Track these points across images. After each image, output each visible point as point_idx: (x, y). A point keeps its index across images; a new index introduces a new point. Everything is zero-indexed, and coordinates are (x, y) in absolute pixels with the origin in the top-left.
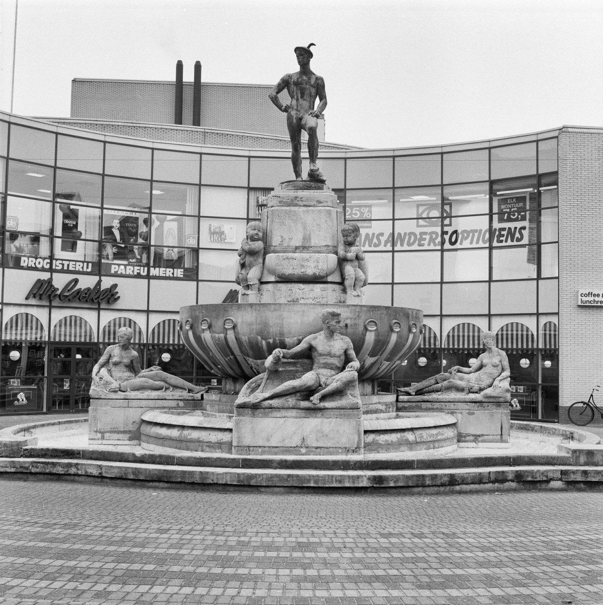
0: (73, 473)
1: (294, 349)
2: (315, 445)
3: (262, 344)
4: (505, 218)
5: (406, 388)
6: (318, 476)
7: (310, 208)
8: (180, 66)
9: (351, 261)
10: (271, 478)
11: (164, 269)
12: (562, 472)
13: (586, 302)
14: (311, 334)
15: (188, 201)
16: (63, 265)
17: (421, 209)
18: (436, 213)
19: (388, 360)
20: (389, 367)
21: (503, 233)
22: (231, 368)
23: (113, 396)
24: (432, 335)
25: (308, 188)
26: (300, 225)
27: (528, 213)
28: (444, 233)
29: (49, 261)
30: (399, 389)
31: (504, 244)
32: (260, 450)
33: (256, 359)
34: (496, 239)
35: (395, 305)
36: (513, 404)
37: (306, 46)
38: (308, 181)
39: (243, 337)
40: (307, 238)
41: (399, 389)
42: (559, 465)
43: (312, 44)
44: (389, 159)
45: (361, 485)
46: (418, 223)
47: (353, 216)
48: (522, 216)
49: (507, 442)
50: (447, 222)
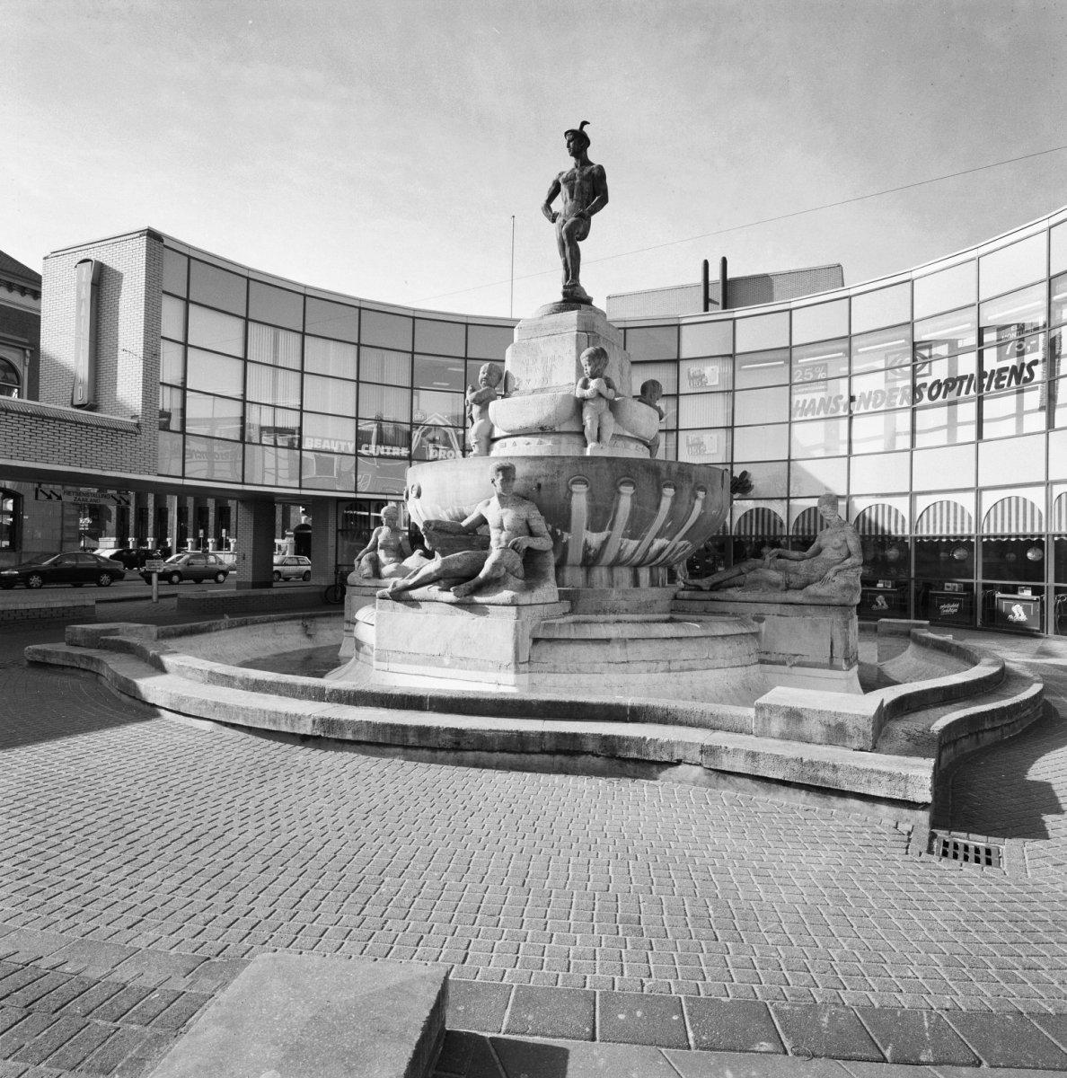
2: (459, 654)
5: (695, 581)
9: (592, 399)
12: (705, 750)
17: (891, 358)
21: (1003, 374)
23: (367, 583)
32: (399, 657)
35: (680, 459)
36: (1015, 612)
37: (577, 127)
43: (584, 123)
45: (302, 732)
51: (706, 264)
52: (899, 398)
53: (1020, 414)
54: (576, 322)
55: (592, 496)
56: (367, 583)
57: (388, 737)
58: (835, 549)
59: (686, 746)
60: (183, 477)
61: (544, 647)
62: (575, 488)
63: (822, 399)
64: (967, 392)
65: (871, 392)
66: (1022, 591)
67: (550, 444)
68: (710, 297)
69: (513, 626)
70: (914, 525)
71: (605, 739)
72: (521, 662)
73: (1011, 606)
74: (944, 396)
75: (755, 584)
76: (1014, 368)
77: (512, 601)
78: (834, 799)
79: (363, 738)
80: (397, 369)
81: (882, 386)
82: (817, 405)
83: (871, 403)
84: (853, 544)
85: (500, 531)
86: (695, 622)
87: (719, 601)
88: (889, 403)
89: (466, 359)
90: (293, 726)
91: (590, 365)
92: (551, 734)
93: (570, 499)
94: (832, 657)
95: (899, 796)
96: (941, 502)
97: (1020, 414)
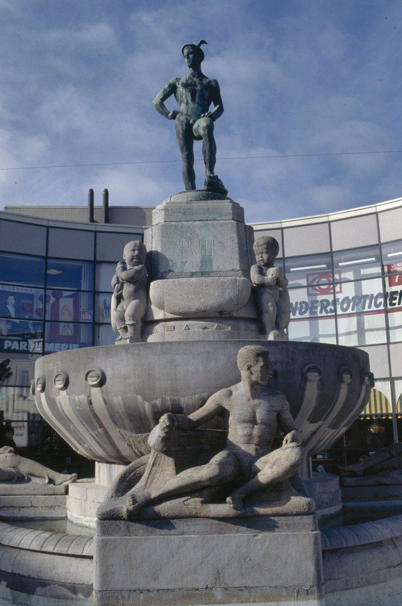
1: (195, 413)
2: (237, 584)
3: (144, 408)
4: (396, 281)
7: (209, 222)
11: (59, 344)
14: (222, 388)
15: (83, 278)
17: (311, 278)
20: (334, 435)
22: (101, 447)
25: (207, 198)
26: (196, 244)
30: (341, 468)
33: (137, 433)
37: (197, 44)
38: (204, 191)
40: (206, 261)
41: (341, 468)
43: (203, 42)
44: (278, 230)
52: (319, 308)
54: (231, 212)
55: (322, 385)
64: (370, 307)
65: (297, 303)
69: (313, 539)
74: (353, 309)
77: (309, 509)
85: (250, 425)
87: (385, 485)
88: (311, 313)
91: (267, 253)
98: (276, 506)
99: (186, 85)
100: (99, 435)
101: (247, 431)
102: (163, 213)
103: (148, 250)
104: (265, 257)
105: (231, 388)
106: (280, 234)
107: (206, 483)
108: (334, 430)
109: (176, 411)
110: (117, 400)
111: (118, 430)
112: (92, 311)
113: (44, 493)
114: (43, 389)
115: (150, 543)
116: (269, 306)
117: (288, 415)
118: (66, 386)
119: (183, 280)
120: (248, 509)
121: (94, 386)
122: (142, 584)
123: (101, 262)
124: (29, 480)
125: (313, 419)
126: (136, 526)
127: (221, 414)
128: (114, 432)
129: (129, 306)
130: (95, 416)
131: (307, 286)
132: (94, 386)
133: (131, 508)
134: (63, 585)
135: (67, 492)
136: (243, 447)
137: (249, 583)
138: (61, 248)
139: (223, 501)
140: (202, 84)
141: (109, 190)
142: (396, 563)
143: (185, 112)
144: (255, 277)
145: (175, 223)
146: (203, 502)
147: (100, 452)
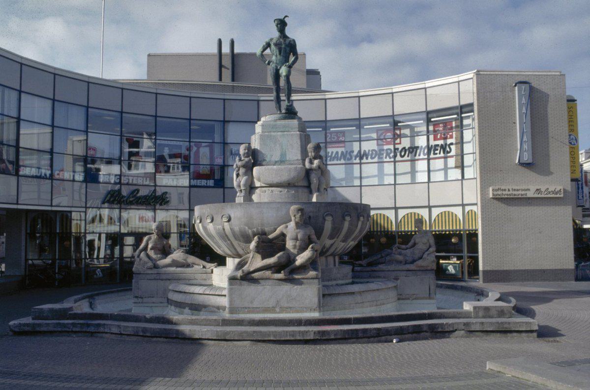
0: (101, 331)
3: (248, 232)
4: (439, 137)
6: (275, 332)
7: (285, 133)
8: (220, 42)
9: (315, 170)
10: (241, 334)
11: (200, 180)
12: (465, 324)
13: (497, 195)
16: (129, 179)
17: (380, 132)
18: (389, 135)
19: (343, 241)
21: (437, 148)
22: (229, 250)
23: (150, 272)
24: (390, 222)
25: (285, 118)
27: (454, 133)
28: (396, 149)
29: (119, 177)
31: (438, 156)
33: (246, 243)
34: (432, 152)
37: (282, 17)
39: (235, 228)
40: (283, 155)
42: (464, 318)
43: (286, 16)
45: (308, 338)
46: (377, 142)
47: (332, 139)
48: (450, 135)
49: (434, 299)
50: (398, 141)
51: (220, 42)
52: (385, 155)
53: (446, 169)
54: (297, 127)
55: (334, 222)
56: (150, 272)
57: (350, 335)
58: (424, 244)
59: (458, 324)
60: (17, 204)
61: (328, 299)
62: (327, 218)
63: (342, 152)
65: (369, 150)
66: (452, 258)
67: (293, 192)
68: (223, 64)
70: (398, 224)
71: (430, 325)
72: (321, 307)
73: (448, 266)
75: (391, 262)
76: (442, 145)
78: (508, 334)
79: (339, 337)
80: (76, 119)
81: (376, 148)
82: (339, 156)
83: (369, 157)
84: (432, 241)
86: (379, 282)
87: (375, 271)
88: (379, 158)
89: (122, 112)
90: (303, 336)
92: (411, 326)
93: (324, 224)
94: (430, 294)
95: (528, 329)
96: (411, 213)
97: (446, 169)
98: (302, 275)
99: (276, 45)
100: (228, 244)
101: (294, 243)
102: (261, 128)
103: (253, 148)
104: (313, 154)
105: (288, 224)
106: (358, 101)
107: (273, 265)
108: (344, 244)
109: (264, 233)
110: (237, 229)
111: (237, 242)
112: (222, 157)
113: (201, 272)
114: (201, 222)
115: (250, 290)
116: (314, 180)
117: (314, 237)
118: (212, 221)
119: (270, 167)
120: (291, 276)
121: (225, 222)
122: (246, 305)
123: (229, 121)
124: (193, 267)
125: (331, 237)
126: (244, 282)
127: (283, 235)
128: (235, 243)
129: (243, 180)
130: (226, 236)
131: (377, 140)
132: (225, 222)
133: (242, 275)
134: (214, 307)
135: (212, 272)
136: (292, 250)
137: (291, 306)
138: (201, 112)
139: (279, 272)
140: (285, 44)
141: (235, 41)
142: (360, 302)
143: (275, 62)
144: (307, 165)
145: (267, 133)
146: (271, 273)
147: (229, 252)
